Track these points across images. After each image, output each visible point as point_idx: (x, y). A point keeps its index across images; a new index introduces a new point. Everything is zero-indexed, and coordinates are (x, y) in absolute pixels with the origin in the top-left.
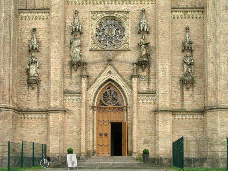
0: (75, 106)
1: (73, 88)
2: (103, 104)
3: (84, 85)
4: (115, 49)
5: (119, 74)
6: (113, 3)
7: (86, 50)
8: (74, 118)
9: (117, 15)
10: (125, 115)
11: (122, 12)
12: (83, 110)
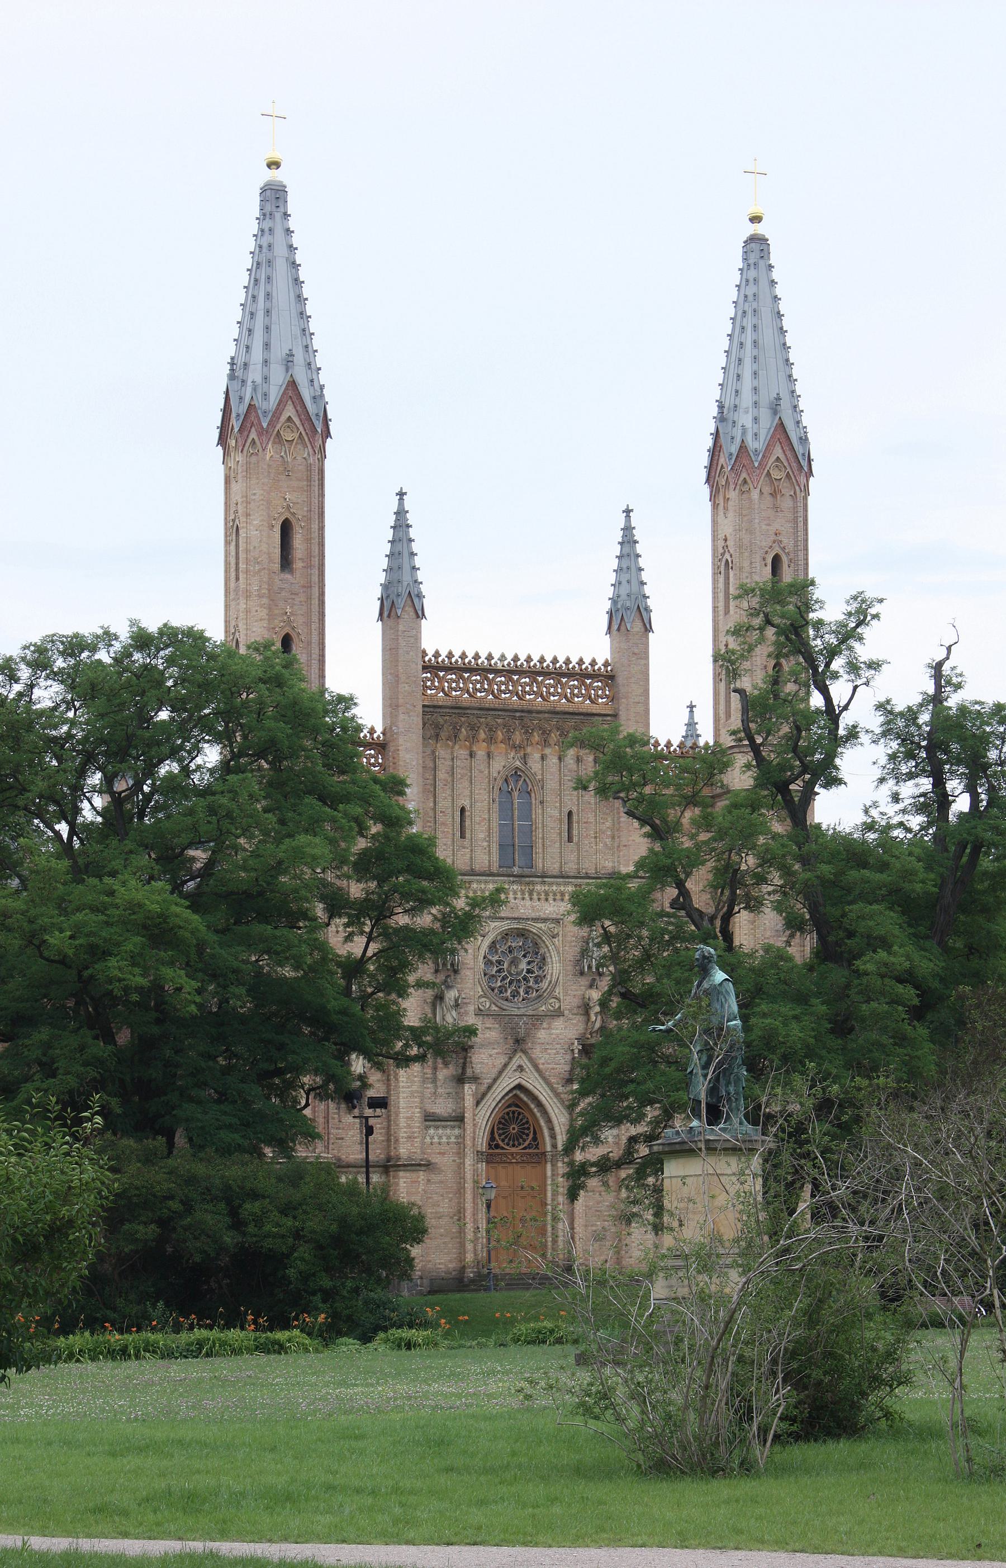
0: (444, 1154)
1: (443, 1107)
2: (497, 1146)
3: (469, 1101)
4: (531, 1013)
6: (527, 896)
7: (466, 1013)
8: (441, 1182)
9: (535, 928)
10: (549, 1173)
11: (545, 920)
12: (468, 1161)
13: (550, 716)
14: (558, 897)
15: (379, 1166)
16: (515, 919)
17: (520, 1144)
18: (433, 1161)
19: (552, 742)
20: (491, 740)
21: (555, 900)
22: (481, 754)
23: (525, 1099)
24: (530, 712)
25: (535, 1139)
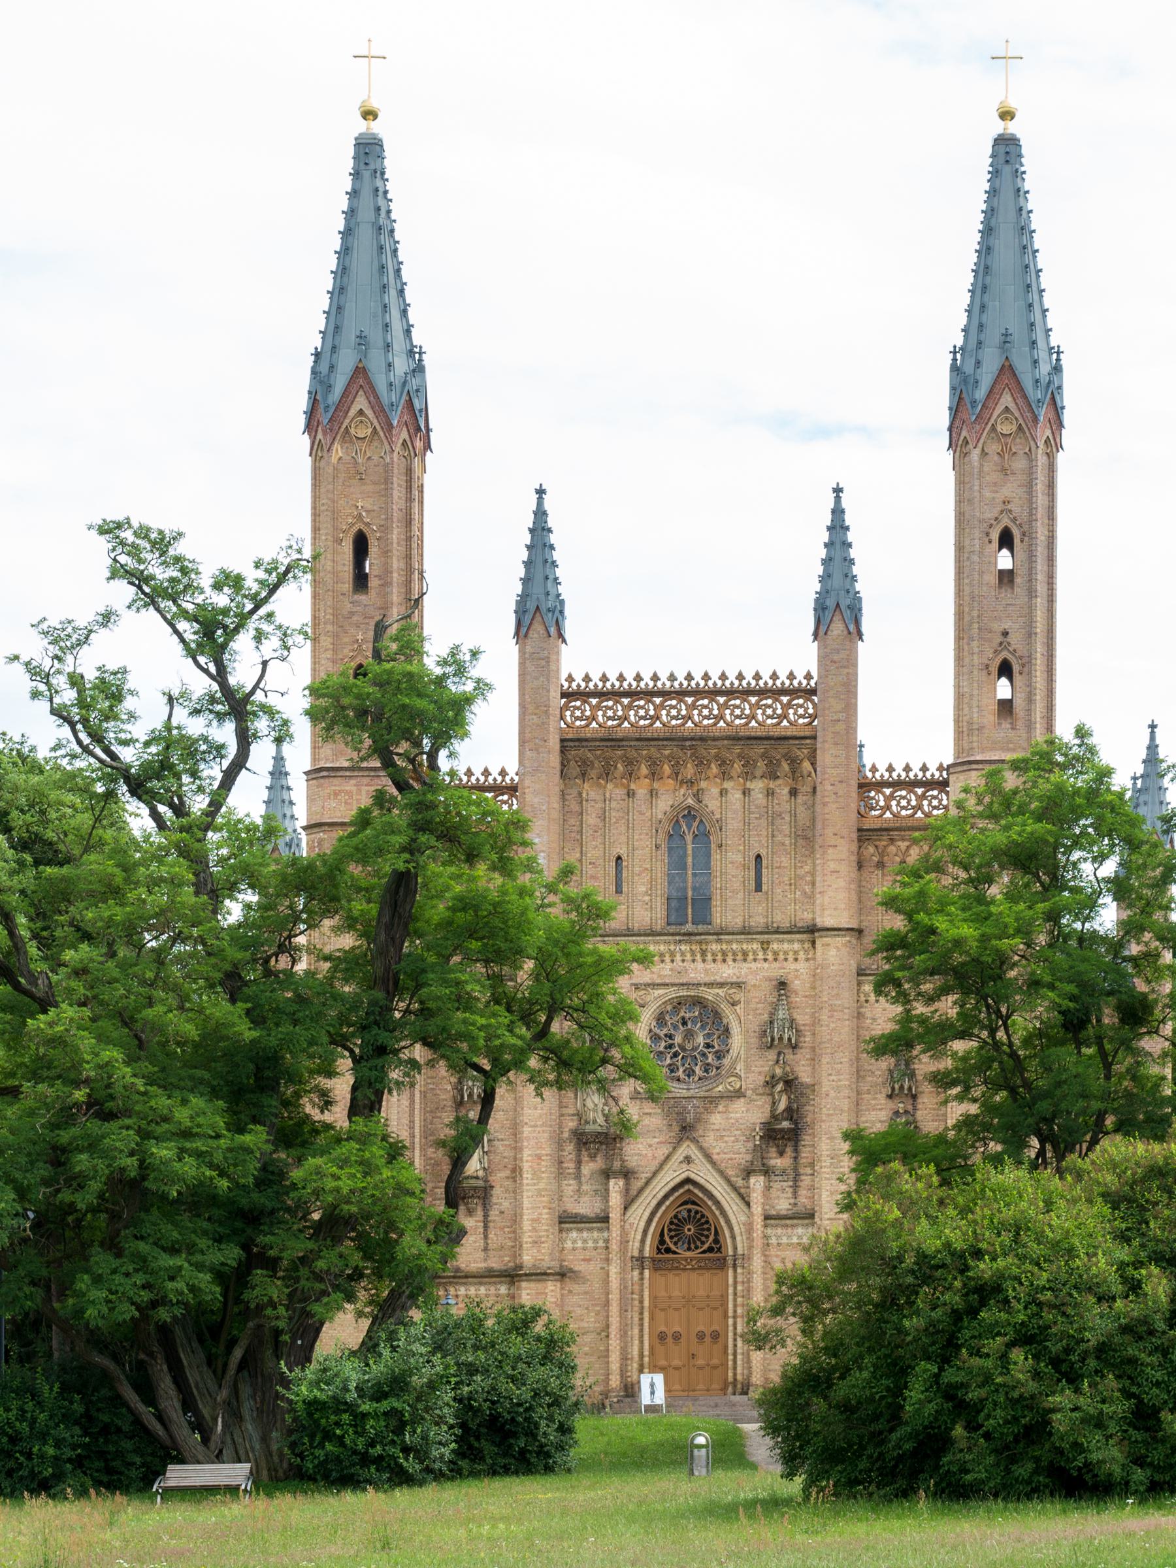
0: (589, 1260)
1: (586, 1207)
2: (668, 1250)
4: (702, 1094)
5: (713, 1163)
6: (698, 957)
8: (586, 1293)
9: (709, 994)
10: (731, 1281)
11: (721, 985)
12: (614, 1270)
13: (731, 742)
14: (740, 957)
15: (506, 1276)
16: (682, 985)
17: (697, 1248)
18: (576, 1269)
19: (734, 774)
20: (654, 775)
21: (734, 960)
22: (641, 791)
23: (700, 1195)
24: (702, 739)
25: (716, 1241)
